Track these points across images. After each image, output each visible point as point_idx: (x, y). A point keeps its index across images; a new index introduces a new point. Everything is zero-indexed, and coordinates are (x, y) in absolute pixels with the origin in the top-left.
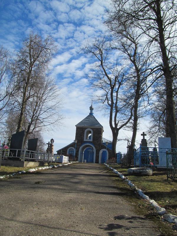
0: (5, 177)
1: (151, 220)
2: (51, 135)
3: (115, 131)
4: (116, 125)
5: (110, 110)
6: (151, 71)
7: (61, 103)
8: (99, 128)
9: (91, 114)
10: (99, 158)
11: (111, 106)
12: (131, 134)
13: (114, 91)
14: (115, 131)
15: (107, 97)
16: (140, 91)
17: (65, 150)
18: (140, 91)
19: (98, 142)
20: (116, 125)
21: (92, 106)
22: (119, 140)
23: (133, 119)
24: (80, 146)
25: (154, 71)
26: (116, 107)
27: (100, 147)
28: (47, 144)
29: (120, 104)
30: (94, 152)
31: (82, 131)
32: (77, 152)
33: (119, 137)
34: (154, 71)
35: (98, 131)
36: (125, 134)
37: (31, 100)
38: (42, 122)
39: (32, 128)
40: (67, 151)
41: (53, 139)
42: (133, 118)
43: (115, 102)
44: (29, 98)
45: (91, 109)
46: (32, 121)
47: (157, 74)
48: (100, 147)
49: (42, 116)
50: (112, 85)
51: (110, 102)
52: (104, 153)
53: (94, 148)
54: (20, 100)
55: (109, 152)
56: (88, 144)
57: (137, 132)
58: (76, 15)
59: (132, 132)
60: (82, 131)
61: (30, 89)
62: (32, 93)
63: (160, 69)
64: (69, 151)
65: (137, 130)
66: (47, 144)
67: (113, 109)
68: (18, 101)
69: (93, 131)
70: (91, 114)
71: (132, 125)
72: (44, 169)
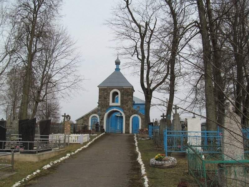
0: (20, 182)
1: (239, 166)
2: (67, 103)
3: (148, 93)
4: (149, 85)
5: (140, 66)
6: (184, 30)
7: (77, 59)
8: (128, 89)
9: (118, 69)
10: (129, 127)
11: (142, 61)
12: (168, 96)
13: (144, 42)
14: (148, 93)
15: (136, 49)
16: (179, 39)
17: (86, 119)
18: (179, 39)
19: (127, 106)
20: (149, 85)
21: (118, 58)
22: (153, 105)
23: (169, 78)
24: (105, 112)
25: (187, 29)
26: (148, 63)
27: (131, 112)
28: (63, 116)
29: (153, 59)
30: (122, 116)
31: (106, 93)
32: (102, 119)
33: (153, 101)
34: (187, 29)
35: (128, 92)
36: (160, 96)
37: (38, 54)
38: (55, 85)
39: (43, 93)
40: (88, 119)
41: (69, 115)
42: (169, 77)
43: (146, 55)
44: (35, 51)
45: (118, 63)
46: (42, 85)
47: (192, 31)
48: (131, 112)
49: (54, 79)
50: (142, 34)
51: (140, 57)
52: (135, 120)
53: (123, 113)
54: (24, 57)
55: (141, 118)
56: (115, 109)
57: (175, 95)
58: (78, 56)
59: (169, 95)
60: (106, 93)
61: (37, 41)
62: (39, 46)
63: (195, 25)
64: (92, 120)
65: (175, 92)
66: (63, 116)
67: (145, 64)
68: (21, 58)
69: (121, 92)
70: (118, 69)
71: (168, 86)
72: (60, 161)
